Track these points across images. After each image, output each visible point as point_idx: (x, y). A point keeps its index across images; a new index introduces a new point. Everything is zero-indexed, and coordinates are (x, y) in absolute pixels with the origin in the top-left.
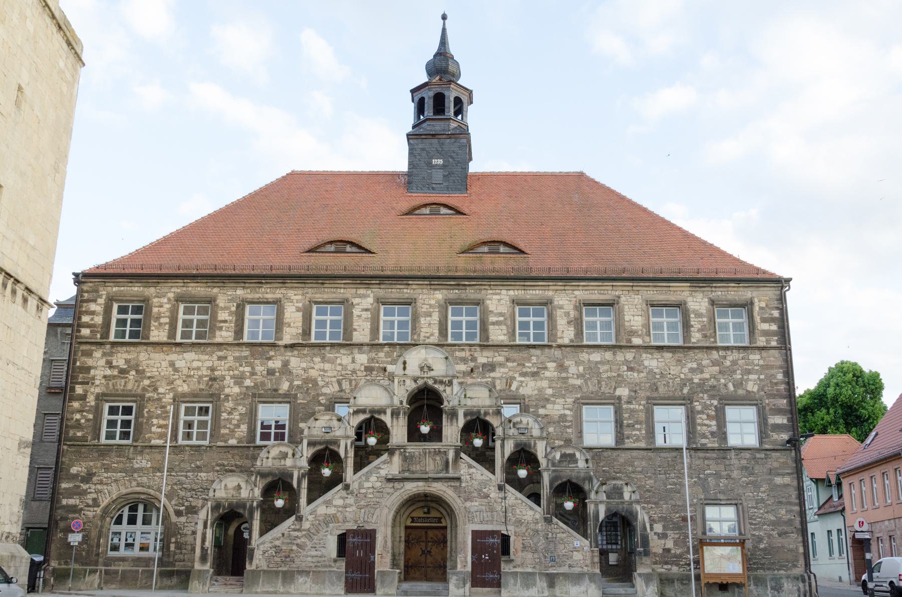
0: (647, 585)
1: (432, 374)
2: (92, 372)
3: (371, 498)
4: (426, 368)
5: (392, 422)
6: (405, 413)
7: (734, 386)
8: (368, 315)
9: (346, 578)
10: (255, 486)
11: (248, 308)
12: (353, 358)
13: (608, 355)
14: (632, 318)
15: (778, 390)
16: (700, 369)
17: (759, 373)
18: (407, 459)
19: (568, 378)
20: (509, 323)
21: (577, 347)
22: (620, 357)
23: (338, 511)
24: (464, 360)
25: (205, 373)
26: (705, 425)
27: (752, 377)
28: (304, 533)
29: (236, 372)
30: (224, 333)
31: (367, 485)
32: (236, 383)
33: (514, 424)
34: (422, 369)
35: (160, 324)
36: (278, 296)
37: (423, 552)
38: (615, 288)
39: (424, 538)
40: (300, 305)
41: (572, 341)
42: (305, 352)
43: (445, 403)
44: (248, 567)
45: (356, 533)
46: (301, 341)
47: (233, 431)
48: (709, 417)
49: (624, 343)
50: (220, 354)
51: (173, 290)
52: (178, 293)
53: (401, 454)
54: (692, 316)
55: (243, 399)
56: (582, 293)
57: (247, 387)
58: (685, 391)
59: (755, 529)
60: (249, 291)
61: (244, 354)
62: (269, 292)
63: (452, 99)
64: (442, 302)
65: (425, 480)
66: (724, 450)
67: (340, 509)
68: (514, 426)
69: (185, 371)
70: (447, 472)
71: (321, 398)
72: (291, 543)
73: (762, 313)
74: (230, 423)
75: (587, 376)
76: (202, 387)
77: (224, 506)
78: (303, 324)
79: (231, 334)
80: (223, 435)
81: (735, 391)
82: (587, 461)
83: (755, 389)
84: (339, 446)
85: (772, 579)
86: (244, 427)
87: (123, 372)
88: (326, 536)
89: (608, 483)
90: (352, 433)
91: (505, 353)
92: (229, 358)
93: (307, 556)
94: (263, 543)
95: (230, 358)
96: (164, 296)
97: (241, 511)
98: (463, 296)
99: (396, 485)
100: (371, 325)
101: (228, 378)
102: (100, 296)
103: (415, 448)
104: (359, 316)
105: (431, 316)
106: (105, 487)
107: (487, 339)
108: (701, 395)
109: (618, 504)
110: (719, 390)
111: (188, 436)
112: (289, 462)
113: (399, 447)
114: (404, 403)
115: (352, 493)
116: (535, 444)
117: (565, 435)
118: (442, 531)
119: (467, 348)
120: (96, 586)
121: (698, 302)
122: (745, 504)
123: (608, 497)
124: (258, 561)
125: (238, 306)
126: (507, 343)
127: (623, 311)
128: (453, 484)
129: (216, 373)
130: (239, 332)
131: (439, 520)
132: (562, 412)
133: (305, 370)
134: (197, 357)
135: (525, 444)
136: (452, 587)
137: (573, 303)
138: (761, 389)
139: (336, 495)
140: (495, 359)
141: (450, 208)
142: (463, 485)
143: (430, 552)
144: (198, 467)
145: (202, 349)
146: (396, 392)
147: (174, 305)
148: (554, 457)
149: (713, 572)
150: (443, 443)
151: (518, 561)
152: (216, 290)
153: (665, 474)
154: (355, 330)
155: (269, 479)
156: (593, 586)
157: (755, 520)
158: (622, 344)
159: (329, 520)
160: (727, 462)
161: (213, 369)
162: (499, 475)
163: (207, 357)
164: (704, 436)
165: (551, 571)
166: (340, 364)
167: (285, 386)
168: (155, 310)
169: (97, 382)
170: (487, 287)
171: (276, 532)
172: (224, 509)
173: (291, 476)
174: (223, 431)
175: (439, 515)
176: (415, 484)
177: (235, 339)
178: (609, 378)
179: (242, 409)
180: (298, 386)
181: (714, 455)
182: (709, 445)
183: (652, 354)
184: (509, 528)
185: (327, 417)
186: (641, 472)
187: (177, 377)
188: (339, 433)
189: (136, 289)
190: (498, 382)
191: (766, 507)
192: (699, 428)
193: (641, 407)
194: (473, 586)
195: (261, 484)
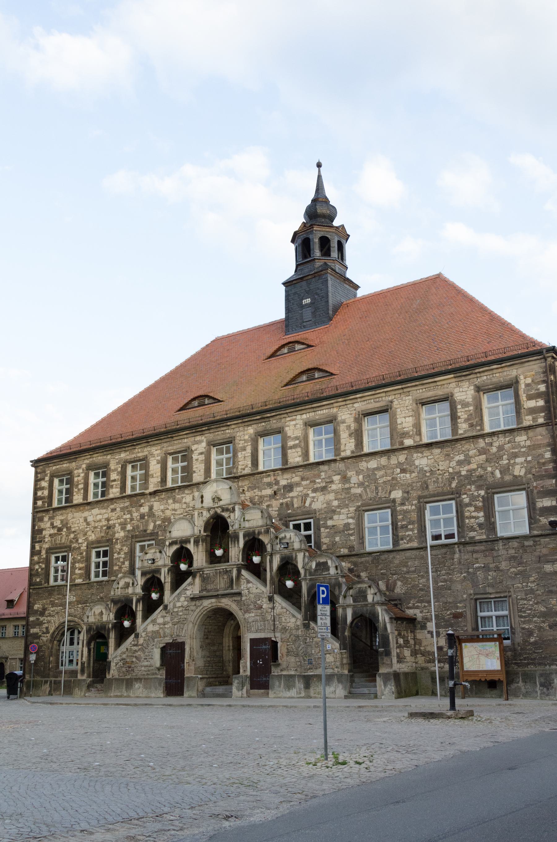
0: (385, 685)
1: (221, 503)
2: (44, 532)
3: (180, 616)
4: (217, 499)
7: (501, 472)
8: (202, 457)
9: (166, 683)
10: (111, 611)
12: (193, 496)
13: (383, 461)
14: (403, 419)
15: (546, 470)
16: (467, 461)
17: (525, 455)
18: (205, 580)
19: (350, 488)
20: (303, 444)
21: (359, 456)
22: (394, 460)
23: (160, 628)
24: (270, 485)
26: (473, 517)
27: (520, 460)
28: (140, 647)
29: (122, 520)
33: (280, 540)
34: (213, 499)
35: (79, 490)
36: (146, 453)
38: (388, 394)
40: (159, 458)
42: (163, 496)
44: (108, 677)
46: (160, 488)
47: (120, 567)
48: (477, 509)
49: (397, 446)
50: (112, 507)
51: (84, 462)
53: (201, 576)
54: (459, 407)
55: (126, 541)
56: (361, 404)
57: (128, 531)
58: (454, 485)
59: (524, 623)
62: (140, 452)
63: (317, 240)
65: (216, 596)
66: (493, 541)
67: (161, 626)
68: (280, 543)
69: (93, 524)
70: (232, 589)
72: (132, 656)
73: (528, 390)
74: (119, 561)
75: (366, 483)
76: (103, 534)
78: (161, 474)
79: (118, 490)
81: (502, 478)
83: (522, 473)
84: (160, 575)
85: (541, 675)
86: (127, 563)
87: (60, 530)
88: (153, 649)
89: (354, 587)
90: (168, 562)
91: (301, 473)
93: (142, 666)
94: (116, 657)
95: (118, 509)
96: (80, 468)
97: (103, 632)
98: (268, 427)
99: (198, 603)
101: (117, 525)
102: (46, 475)
104: (197, 460)
105: (245, 450)
106: (52, 618)
108: (469, 487)
109: (362, 606)
110: (486, 480)
111: (97, 575)
112: (130, 590)
113: (200, 570)
114: (202, 533)
116: (296, 556)
117: (349, 543)
119: (272, 473)
120: (47, 692)
121: (464, 392)
122: (514, 596)
123: (354, 601)
127: (395, 415)
128: (236, 598)
130: (123, 488)
132: (346, 521)
136: (234, 690)
137: (353, 415)
138: (528, 472)
139: (158, 615)
140: (292, 480)
141: (303, 344)
148: (311, 566)
149: (472, 669)
151: (284, 665)
152: (109, 457)
154: (194, 472)
155: (119, 605)
156: (340, 686)
157: (524, 612)
159: (156, 634)
160: (495, 554)
161: (108, 520)
162: (266, 590)
163: (104, 511)
164: (472, 529)
165: (310, 673)
168: (76, 479)
169: (46, 540)
171: (123, 648)
172: (94, 631)
176: (209, 601)
177: (121, 494)
178: (384, 482)
179: (126, 549)
181: (483, 548)
182: (477, 538)
183: (422, 453)
184: (278, 635)
186: (414, 571)
187: (88, 529)
188: (160, 563)
189: (65, 465)
190: (295, 500)
191: (535, 598)
192: (467, 521)
193: (414, 507)
195: (114, 609)
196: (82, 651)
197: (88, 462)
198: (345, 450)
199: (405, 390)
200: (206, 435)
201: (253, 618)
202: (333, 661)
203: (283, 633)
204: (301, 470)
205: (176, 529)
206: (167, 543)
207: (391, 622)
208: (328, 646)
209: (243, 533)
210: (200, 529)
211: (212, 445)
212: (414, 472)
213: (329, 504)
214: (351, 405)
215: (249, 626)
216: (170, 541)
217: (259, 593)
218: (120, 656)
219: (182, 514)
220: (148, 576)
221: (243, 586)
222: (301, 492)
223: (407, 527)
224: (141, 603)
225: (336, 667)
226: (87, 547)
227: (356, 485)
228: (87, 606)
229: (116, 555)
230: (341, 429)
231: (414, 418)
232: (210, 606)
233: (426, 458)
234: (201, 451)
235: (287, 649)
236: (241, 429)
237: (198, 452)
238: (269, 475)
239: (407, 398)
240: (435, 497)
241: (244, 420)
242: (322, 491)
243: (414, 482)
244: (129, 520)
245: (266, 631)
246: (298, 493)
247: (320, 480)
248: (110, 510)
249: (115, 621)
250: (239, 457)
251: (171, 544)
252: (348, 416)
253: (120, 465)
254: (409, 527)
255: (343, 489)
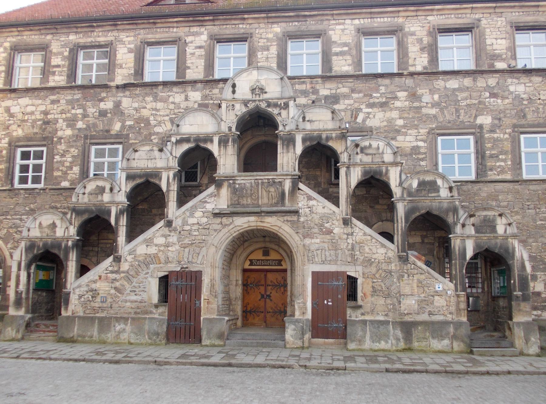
1: (265, 96)
3: (196, 235)
5: (220, 151)
6: (234, 141)
8: (202, 52)
10: (71, 224)
11: (81, 54)
13: (467, 81)
14: (494, 41)
19: (421, 108)
20: (354, 52)
21: (432, 73)
22: (481, 82)
23: (160, 251)
24: (305, 93)
25: (38, 117)
29: (69, 115)
30: (57, 78)
31: (191, 221)
32: (68, 126)
34: (253, 90)
36: (112, 38)
37: (263, 296)
39: (263, 282)
40: (132, 46)
41: (425, 68)
42: (137, 92)
43: (281, 128)
44: (63, 313)
45: (179, 275)
46: (132, 82)
47: (65, 173)
49: (485, 68)
52: (14, 42)
53: (229, 186)
55: (75, 141)
57: (80, 129)
60: (81, 35)
61: (76, 97)
62: (100, 36)
64: (280, 35)
67: (162, 248)
68: (362, 151)
69: (20, 116)
70: (283, 204)
71: (153, 137)
74: (63, 166)
75: (444, 104)
76: (35, 130)
77: (39, 246)
79: (64, 78)
80: (56, 178)
82: (451, 189)
84: (160, 179)
86: (76, 169)
88: (146, 278)
90: (174, 164)
91: (350, 83)
92: (61, 101)
93: (126, 301)
94: (79, 286)
97: (56, 251)
98: (303, 28)
99: (225, 220)
100: (205, 62)
101: (61, 121)
103: (247, 180)
104: (193, 54)
105: (268, 49)
107: (330, 70)
111: (24, 180)
112: (106, 197)
113: (230, 178)
114: (234, 129)
115: (175, 230)
116: (387, 171)
118: (282, 274)
119: (308, 80)
123: (477, 231)
124: (74, 306)
125: (71, 51)
126: (352, 73)
127: (484, 35)
128: (289, 218)
129: (49, 117)
130: (72, 74)
131: (279, 262)
132: (415, 144)
133: (136, 109)
134: (30, 102)
135: (376, 172)
137: (427, 28)
139: (156, 233)
140: (338, 91)
142: (302, 219)
143: (269, 296)
144: (32, 210)
145: (36, 93)
146: (224, 118)
147: (10, 54)
148: (411, 185)
150: (278, 173)
152: (49, 37)
153: (535, 208)
155: (86, 217)
158: (483, 69)
159: (149, 261)
161: (46, 113)
163: (40, 102)
166: (173, 103)
167: (117, 127)
170: (329, 18)
172: (38, 250)
173: (109, 213)
174: (57, 174)
175: (279, 258)
177: (67, 83)
178: (468, 105)
179: (74, 151)
180: (130, 126)
183: (517, 78)
185: (147, 148)
186: (506, 207)
187: (11, 122)
193: (507, 136)
194: (313, 337)
196: (18, 277)
197: (14, 40)
198: (414, 65)
199: (497, 10)
200: (207, 27)
201: (317, 245)
202: (445, 304)
203: (366, 266)
204: (351, 80)
205: (187, 123)
206: (173, 139)
207: (530, 261)
208: (437, 287)
209: (301, 135)
210: (230, 125)
211: (215, 39)
212: (507, 98)
213: (391, 122)
214: (423, 17)
215: (310, 254)
216: (178, 138)
217: (328, 214)
218: (88, 285)
219: (167, 115)
220: (139, 181)
221: (302, 203)
222: (350, 105)
223: (497, 157)
224: (125, 215)
225: (450, 313)
226: (10, 144)
227: (430, 105)
228: (6, 219)
229: (57, 158)
230: (409, 42)
231: (509, 41)
232: (246, 225)
233: (523, 85)
234: (199, 45)
235: (373, 287)
236: (262, 25)
237: (195, 45)
238: (304, 82)
239: (499, 19)
240: (534, 127)
241: (270, 15)
242: (381, 107)
243: (507, 109)
244: (80, 116)
245: (339, 262)
246: (346, 106)
247: (379, 95)
248: (49, 101)
249: (78, 238)
250: (259, 57)
251: (179, 142)
252: (419, 28)
253: (68, 49)
254: (500, 157)
255: (411, 107)
